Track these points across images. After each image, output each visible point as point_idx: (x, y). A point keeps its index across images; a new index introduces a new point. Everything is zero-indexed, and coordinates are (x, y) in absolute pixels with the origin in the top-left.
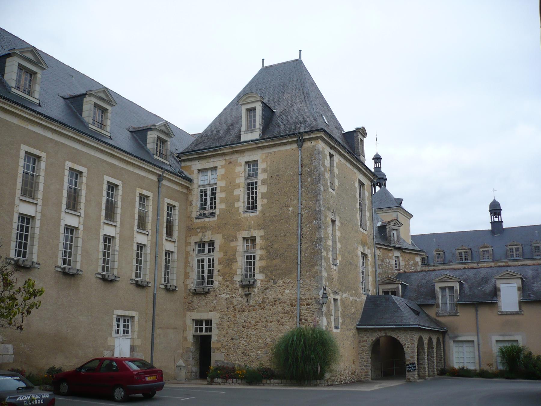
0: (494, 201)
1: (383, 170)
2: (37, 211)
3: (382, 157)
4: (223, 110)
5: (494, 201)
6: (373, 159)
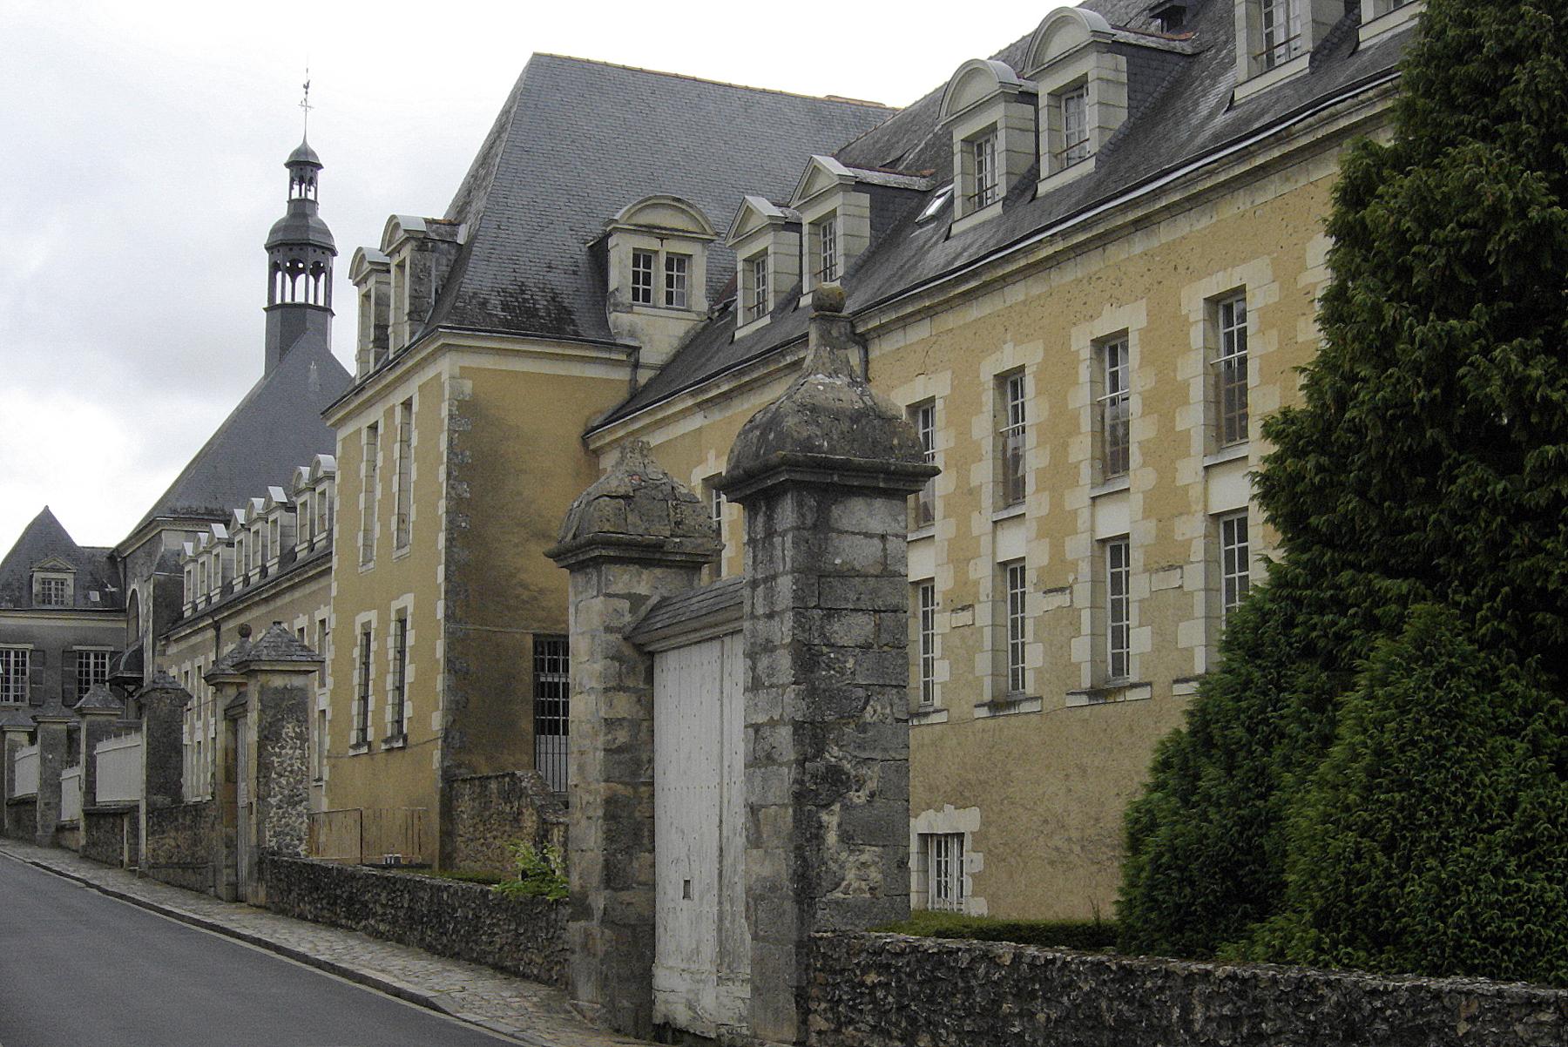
0: (46, 512)
1: (324, 214)
2: (876, 541)
3: (321, 162)
4: (619, 62)
5: (46, 512)
6: (288, 165)
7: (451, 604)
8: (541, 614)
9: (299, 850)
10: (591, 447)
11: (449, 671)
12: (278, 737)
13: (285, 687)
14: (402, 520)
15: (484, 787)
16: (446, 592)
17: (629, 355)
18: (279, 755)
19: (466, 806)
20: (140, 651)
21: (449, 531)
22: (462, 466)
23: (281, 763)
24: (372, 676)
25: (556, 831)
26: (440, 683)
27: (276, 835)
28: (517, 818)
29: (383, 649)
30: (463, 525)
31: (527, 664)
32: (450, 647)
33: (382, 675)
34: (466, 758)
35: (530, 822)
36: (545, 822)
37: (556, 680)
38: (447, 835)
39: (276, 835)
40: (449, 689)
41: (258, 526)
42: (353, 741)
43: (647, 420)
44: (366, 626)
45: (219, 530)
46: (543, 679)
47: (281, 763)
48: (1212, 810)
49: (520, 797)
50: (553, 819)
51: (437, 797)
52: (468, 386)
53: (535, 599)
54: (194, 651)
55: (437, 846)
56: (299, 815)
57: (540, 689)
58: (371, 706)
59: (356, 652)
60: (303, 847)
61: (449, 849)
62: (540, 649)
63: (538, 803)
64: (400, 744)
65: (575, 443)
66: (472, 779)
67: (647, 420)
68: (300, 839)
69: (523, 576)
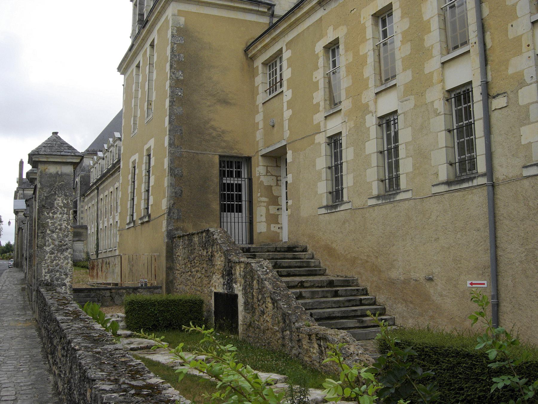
7: (171, 137)
8: (223, 144)
9: (65, 281)
10: (249, 56)
11: (171, 175)
12: (52, 206)
13: (57, 173)
14: (149, 104)
15: (191, 240)
16: (170, 131)
17: (269, 9)
18: (53, 218)
19: (180, 252)
20: (77, 201)
21: (171, 96)
22: (179, 62)
23: (53, 224)
24: (136, 187)
25: (238, 267)
26: (166, 182)
27: (50, 271)
28: (211, 259)
29: (141, 172)
30: (179, 94)
31: (216, 171)
32: (171, 162)
33: (140, 186)
34: (180, 225)
35: (219, 261)
36: (230, 261)
37: (232, 182)
38: (170, 269)
39: (50, 271)
40: (171, 185)
41: (111, 149)
42: (128, 221)
43: (285, 25)
44: (134, 162)
45: (100, 154)
46: (224, 182)
47: (53, 224)
48: (189, 263)
49: (213, 245)
50: (235, 259)
51: (165, 247)
52: (182, 20)
53: (220, 136)
54: (92, 199)
55: (165, 276)
56: (66, 258)
57: (224, 187)
58: (135, 203)
59: (130, 176)
60: (68, 279)
61: (171, 278)
62: (223, 165)
63: (225, 249)
64: (147, 219)
65: (241, 54)
66: (183, 236)
67: (285, 25)
68: (66, 275)
69: (212, 123)
